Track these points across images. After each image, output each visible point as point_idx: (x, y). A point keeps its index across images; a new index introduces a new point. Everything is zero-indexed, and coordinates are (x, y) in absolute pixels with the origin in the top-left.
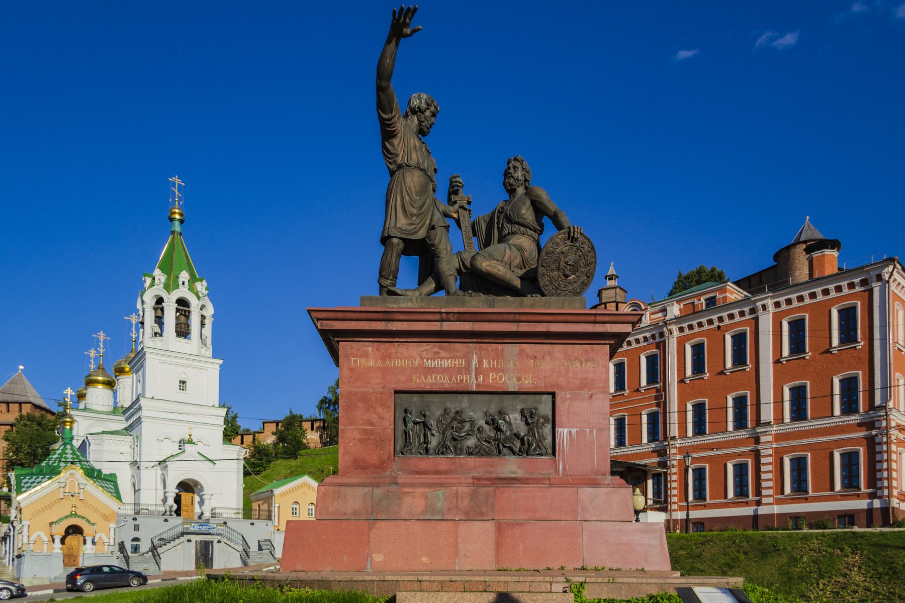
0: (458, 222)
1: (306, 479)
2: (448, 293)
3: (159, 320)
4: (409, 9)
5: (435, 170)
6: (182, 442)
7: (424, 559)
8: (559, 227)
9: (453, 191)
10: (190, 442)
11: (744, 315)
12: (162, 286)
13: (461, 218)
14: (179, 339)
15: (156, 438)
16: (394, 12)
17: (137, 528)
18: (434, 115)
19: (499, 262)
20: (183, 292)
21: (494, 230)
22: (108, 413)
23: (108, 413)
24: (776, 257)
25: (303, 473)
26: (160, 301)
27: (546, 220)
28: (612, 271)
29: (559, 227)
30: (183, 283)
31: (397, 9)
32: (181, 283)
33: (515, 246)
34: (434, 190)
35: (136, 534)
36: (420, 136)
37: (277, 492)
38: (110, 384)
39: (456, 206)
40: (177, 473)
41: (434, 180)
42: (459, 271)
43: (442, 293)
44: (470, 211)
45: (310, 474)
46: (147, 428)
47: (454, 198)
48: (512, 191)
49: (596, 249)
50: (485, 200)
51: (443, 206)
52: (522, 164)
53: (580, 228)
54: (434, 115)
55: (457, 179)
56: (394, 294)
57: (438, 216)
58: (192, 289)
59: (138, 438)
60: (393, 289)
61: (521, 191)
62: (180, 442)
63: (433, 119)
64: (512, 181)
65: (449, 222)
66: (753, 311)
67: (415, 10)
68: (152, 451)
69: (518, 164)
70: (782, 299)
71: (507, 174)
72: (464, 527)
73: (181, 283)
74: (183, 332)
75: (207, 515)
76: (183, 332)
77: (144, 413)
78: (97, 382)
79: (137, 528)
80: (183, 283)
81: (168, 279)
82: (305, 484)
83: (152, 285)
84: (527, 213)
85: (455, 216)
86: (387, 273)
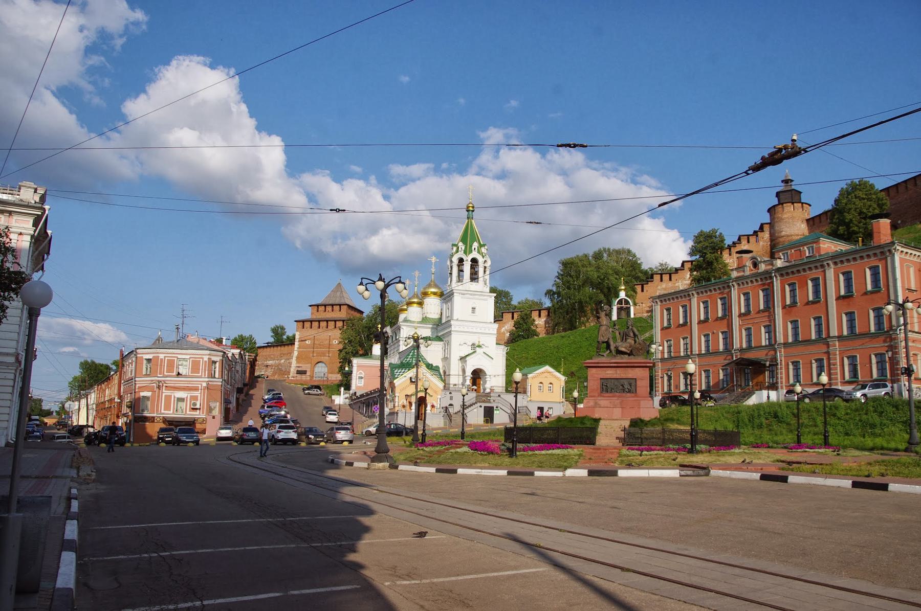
3: (461, 271)
10: (479, 346)
15: (459, 344)
17: (451, 398)
20: (475, 254)
21: (624, 337)
22: (419, 323)
23: (419, 323)
26: (461, 261)
35: (451, 402)
38: (420, 304)
46: (455, 339)
58: (479, 252)
59: (449, 343)
68: (457, 350)
72: (85, 424)
74: (474, 277)
75: (488, 391)
76: (474, 277)
77: (453, 328)
78: (414, 303)
79: (451, 398)
81: (466, 248)
83: (457, 251)
84: (632, 334)
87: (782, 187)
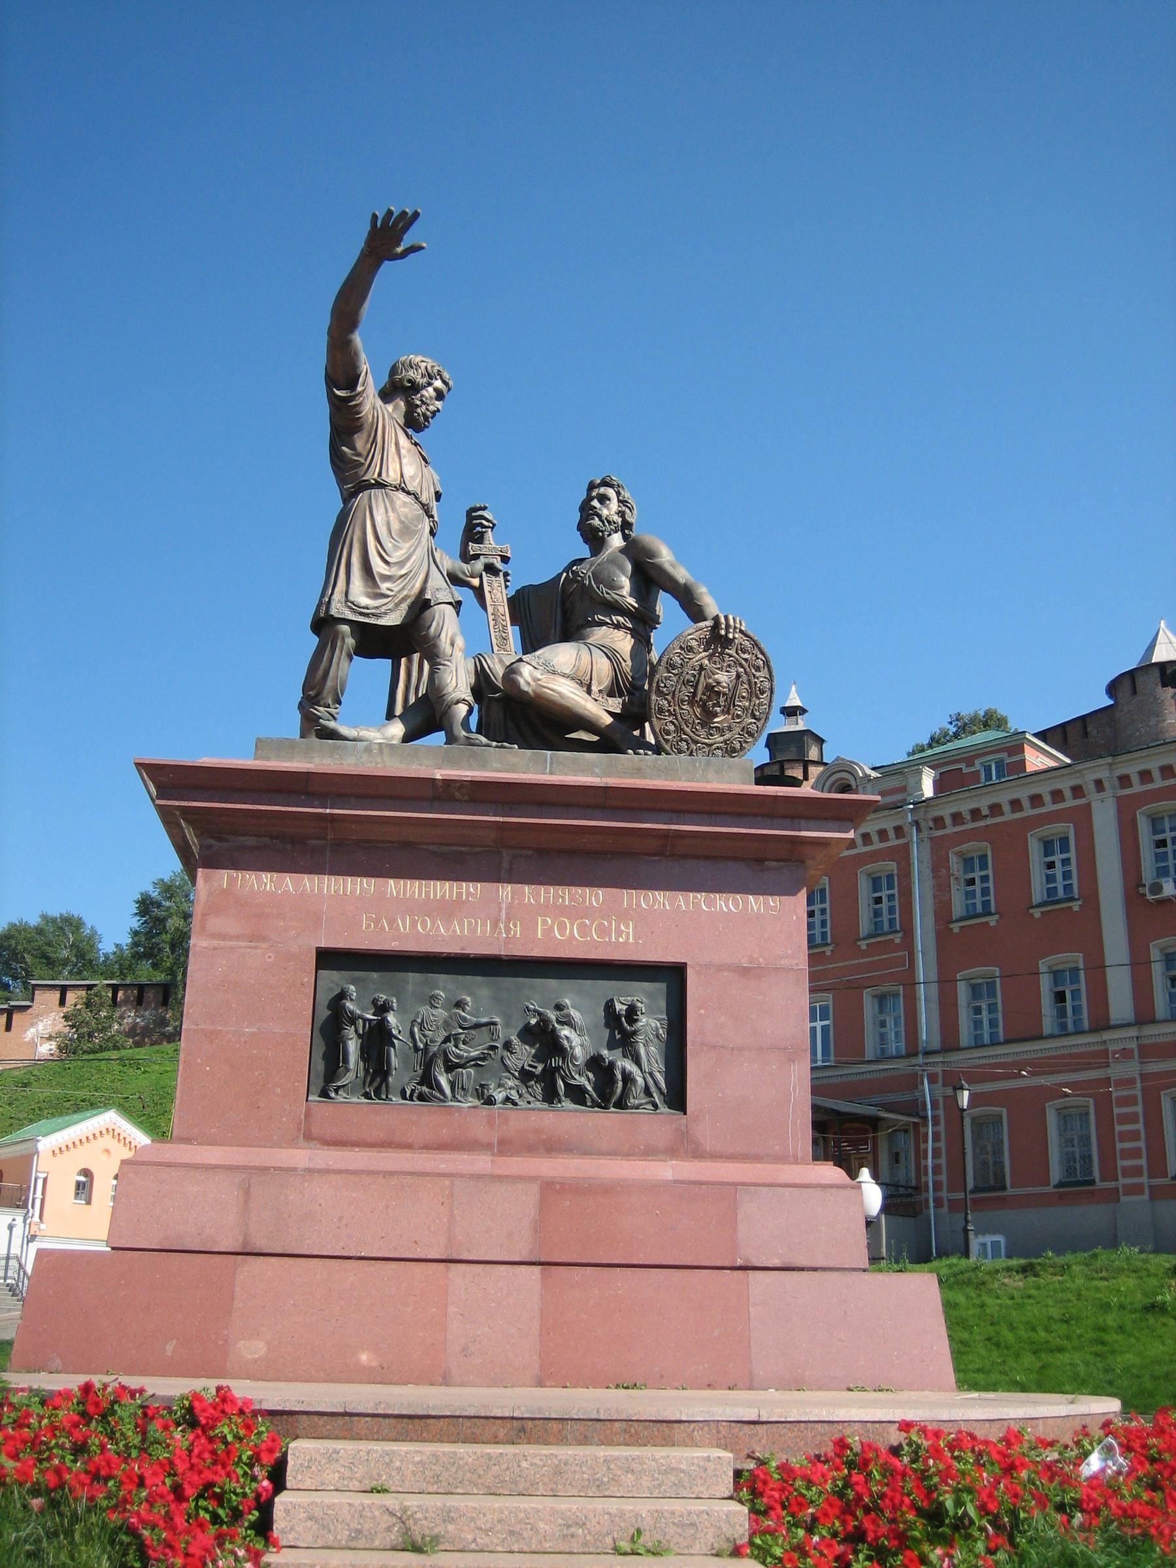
0: (479, 592)
1: (111, 1118)
2: (451, 739)
4: (404, 213)
5: (438, 496)
7: (364, 1357)
8: (695, 612)
9: (473, 531)
11: (1152, 780)
13: (486, 588)
16: (375, 217)
18: (440, 396)
19: (568, 674)
21: (552, 613)
24: (1113, 688)
25: (106, 1105)
27: (665, 605)
28: (794, 701)
29: (695, 612)
31: (380, 215)
33: (601, 647)
34: (432, 533)
36: (410, 431)
37: (45, 1144)
39: (479, 565)
41: (435, 513)
42: (477, 691)
43: (439, 738)
44: (506, 574)
45: (126, 1110)
47: (473, 548)
48: (594, 539)
49: (772, 664)
50: (542, 552)
51: (449, 562)
52: (618, 494)
53: (740, 621)
54: (440, 396)
55: (485, 514)
56: (333, 735)
57: (437, 581)
60: (332, 724)
61: (616, 541)
63: (439, 404)
64: (596, 522)
65: (459, 593)
66: (899, 831)
67: (416, 215)
69: (611, 492)
70: (1132, 769)
71: (587, 510)
82: (111, 1131)
85: (476, 582)
86: (316, 692)
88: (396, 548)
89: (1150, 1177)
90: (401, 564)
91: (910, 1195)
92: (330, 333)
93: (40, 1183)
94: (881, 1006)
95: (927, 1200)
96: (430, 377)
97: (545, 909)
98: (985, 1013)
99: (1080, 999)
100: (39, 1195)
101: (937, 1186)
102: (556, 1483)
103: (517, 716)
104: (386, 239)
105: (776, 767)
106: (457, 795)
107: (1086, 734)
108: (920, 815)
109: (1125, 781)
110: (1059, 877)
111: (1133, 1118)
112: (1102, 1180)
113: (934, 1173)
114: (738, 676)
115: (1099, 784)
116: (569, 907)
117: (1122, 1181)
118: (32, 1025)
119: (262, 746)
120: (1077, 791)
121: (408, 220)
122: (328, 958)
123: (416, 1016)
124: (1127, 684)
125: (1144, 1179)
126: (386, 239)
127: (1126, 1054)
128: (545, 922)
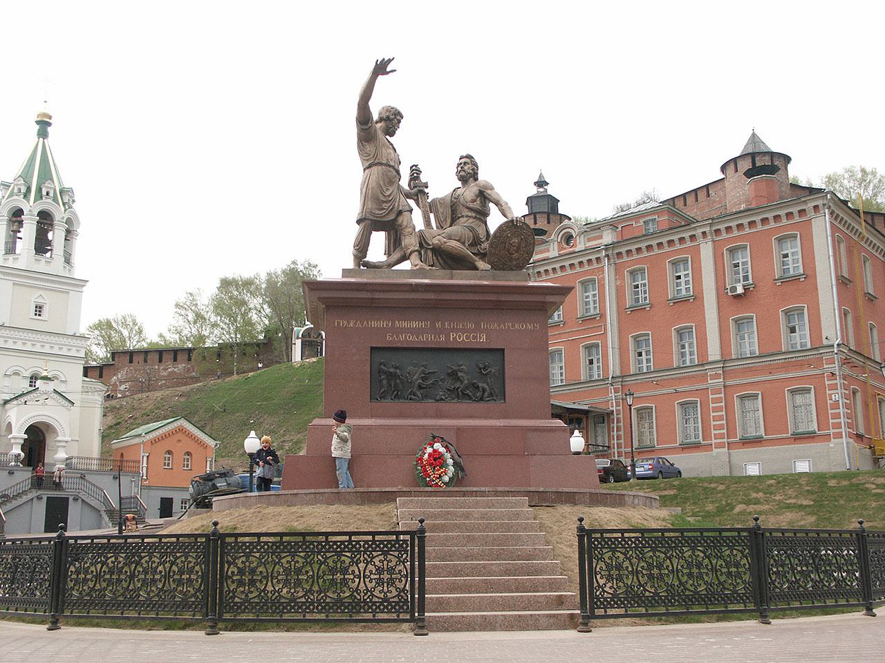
6: (34, 378)
12: (22, 196)
14: (38, 257)
24: (723, 168)
30: (48, 194)
32: (44, 193)
40: (19, 419)
50: (442, 184)
58: (55, 200)
62: (31, 378)
73: (44, 193)
76: (42, 245)
80: (48, 194)
82: (181, 430)
87: (534, 191)
88: (387, 190)
89: (728, 439)
90: (390, 195)
91: (606, 451)
92: (358, 105)
93: (145, 458)
94: (589, 352)
95: (614, 453)
96: (395, 115)
97: (453, 330)
98: (687, 349)
99: (693, 347)
100: (145, 465)
101: (619, 446)
102: (477, 505)
103: (447, 259)
104: (381, 68)
105: (532, 216)
106: (420, 290)
107: (708, 195)
108: (610, 252)
109: (718, 232)
110: (683, 284)
111: (715, 410)
112: (703, 441)
113: (617, 439)
114: (522, 239)
115: (704, 233)
116: (462, 329)
117: (714, 441)
118: (114, 375)
119: (346, 272)
120: (693, 237)
121: (390, 61)
122: (373, 349)
123: (413, 370)
124: (732, 166)
125: (725, 440)
126: (381, 68)
127: (716, 376)
128: (453, 335)
